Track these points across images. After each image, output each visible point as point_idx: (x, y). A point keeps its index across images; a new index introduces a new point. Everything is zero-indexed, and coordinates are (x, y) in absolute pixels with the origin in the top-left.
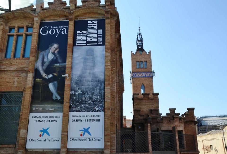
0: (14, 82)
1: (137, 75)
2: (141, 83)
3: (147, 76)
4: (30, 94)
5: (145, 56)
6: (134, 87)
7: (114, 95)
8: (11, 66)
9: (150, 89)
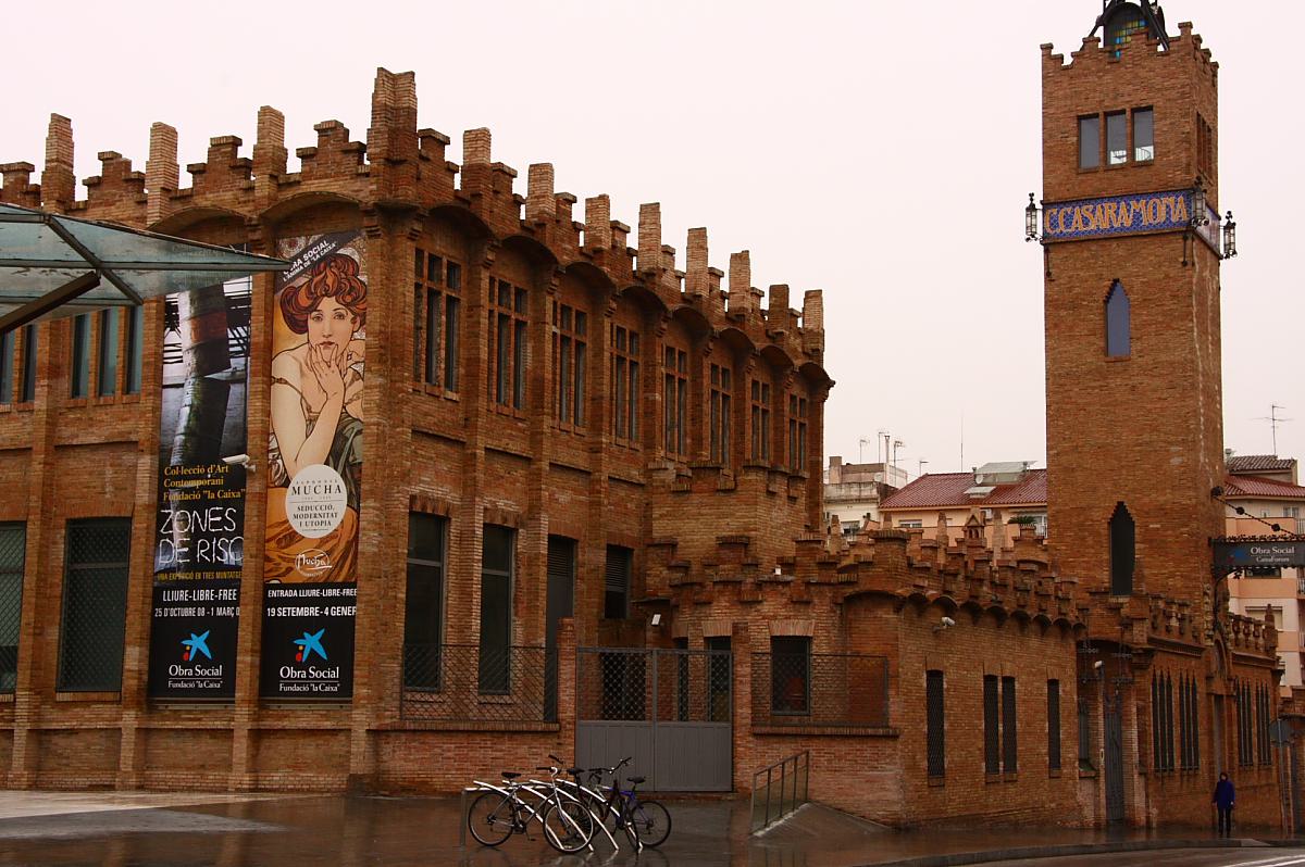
0: (103, 487)
1: (1077, 217)
2: (1105, 273)
3: (1147, 219)
4: (147, 528)
5: (1143, 73)
6: (1057, 308)
7: (394, 528)
8: (91, 426)
9: (1164, 314)
